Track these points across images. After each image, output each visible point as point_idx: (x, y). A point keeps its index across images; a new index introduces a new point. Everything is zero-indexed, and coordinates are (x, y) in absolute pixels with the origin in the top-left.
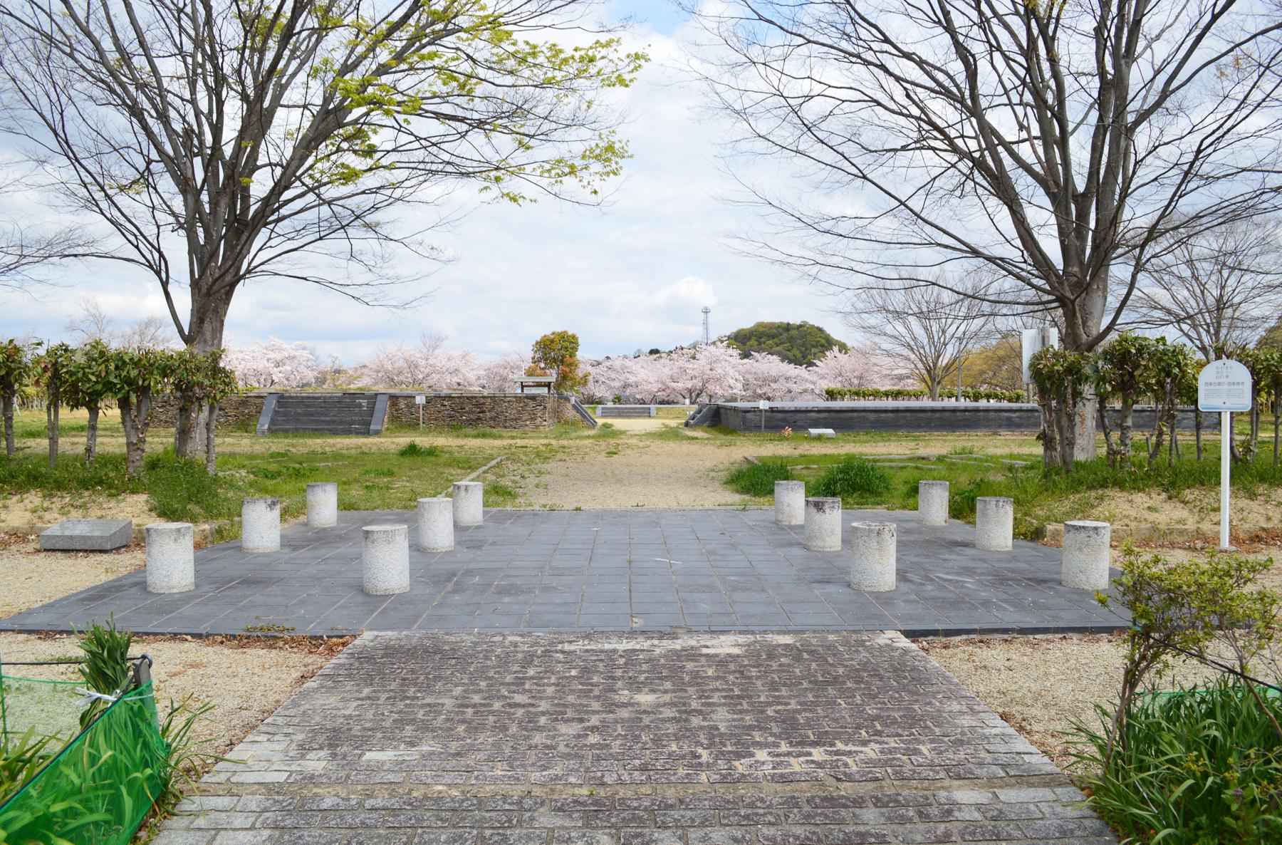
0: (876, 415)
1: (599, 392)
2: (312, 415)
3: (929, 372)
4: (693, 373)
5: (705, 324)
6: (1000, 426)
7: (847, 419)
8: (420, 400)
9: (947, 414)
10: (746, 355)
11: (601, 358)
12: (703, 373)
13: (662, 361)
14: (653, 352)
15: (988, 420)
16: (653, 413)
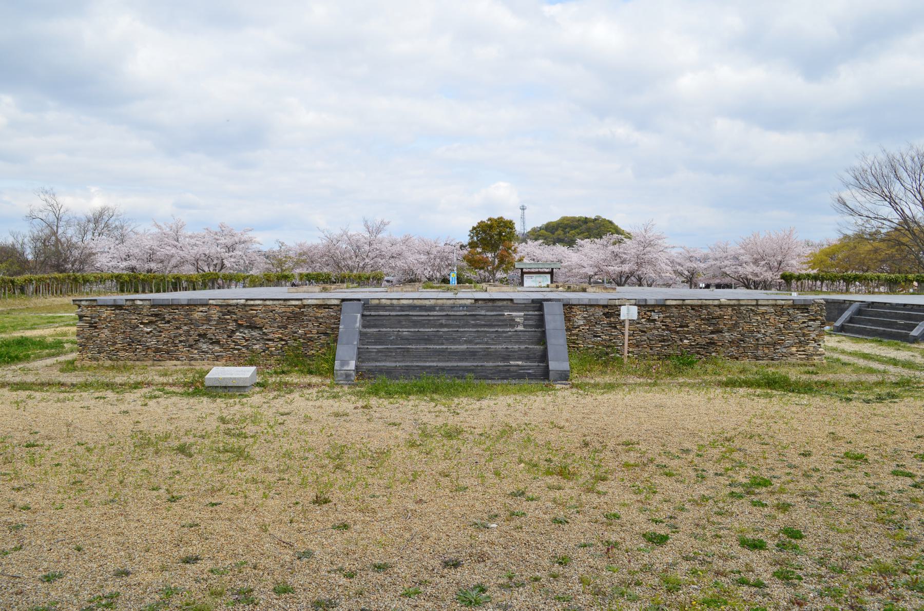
2: (428, 340)
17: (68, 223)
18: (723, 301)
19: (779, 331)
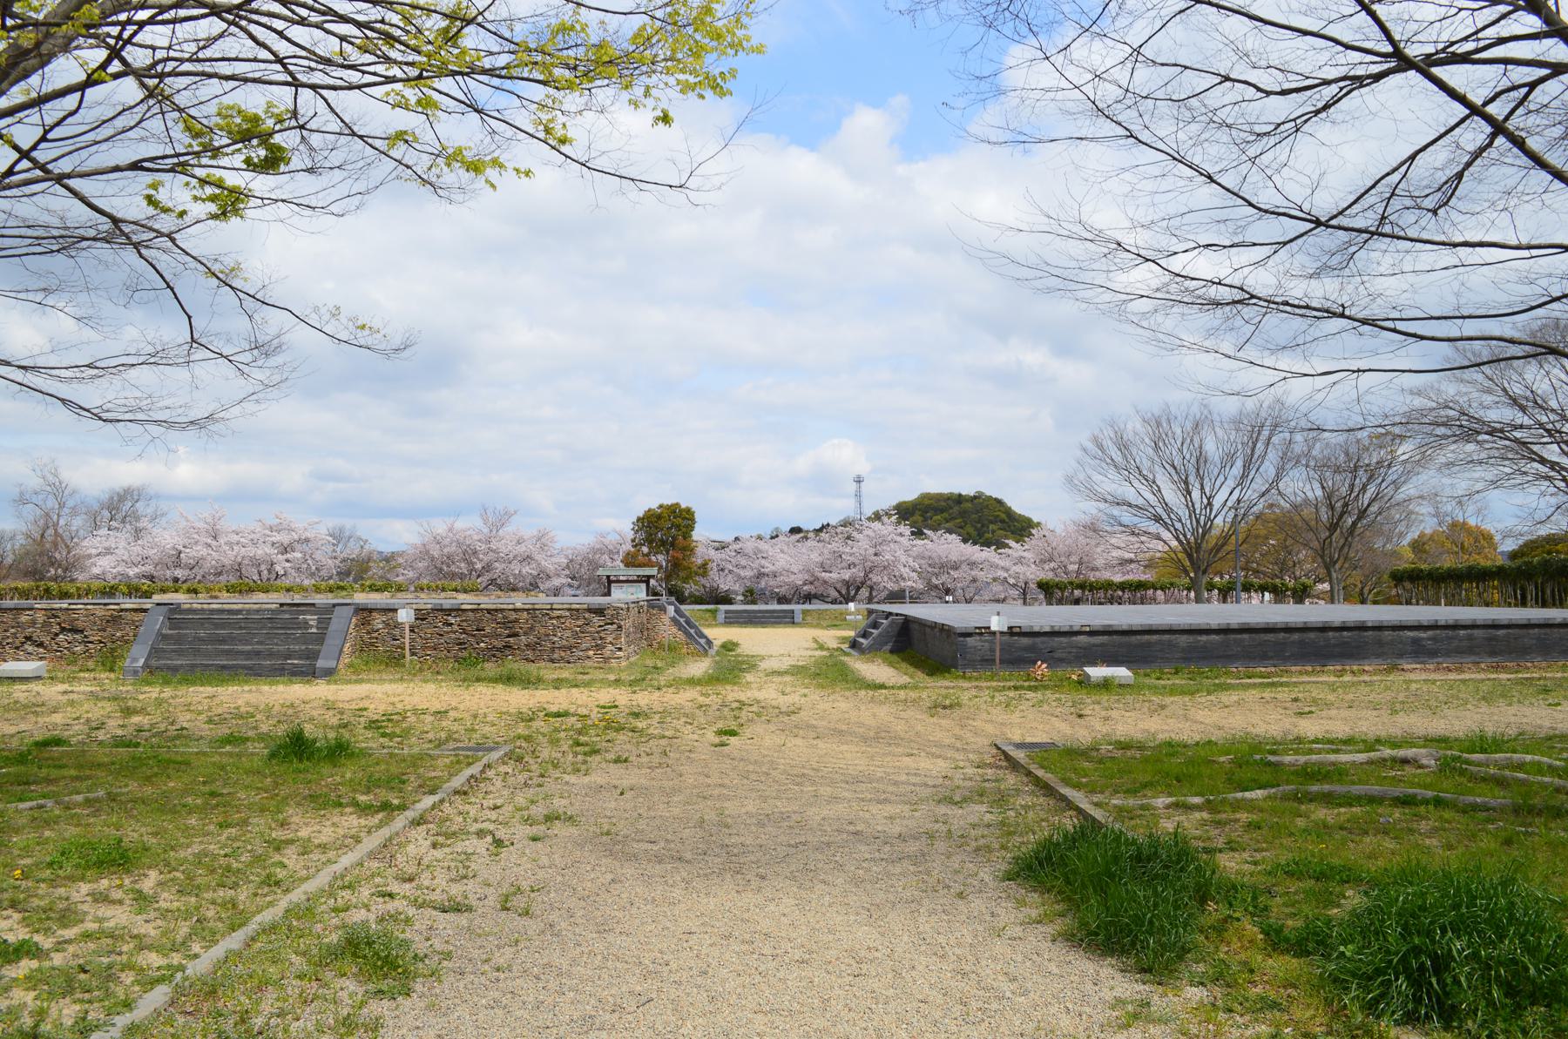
0: (1191, 638)
1: (725, 584)
2: (223, 641)
3: (1190, 556)
4: (852, 559)
5: (858, 495)
6: (1401, 656)
7: (1142, 645)
8: (405, 616)
9: (1312, 635)
10: (918, 534)
11: (729, 538)
12: (865, 560)
13: (810, 543)
14: (795, 530)
15: (1380, 643)
16: (798, 618)
17: (74, 512)
18: (519, 605)
19: (576, 635)
